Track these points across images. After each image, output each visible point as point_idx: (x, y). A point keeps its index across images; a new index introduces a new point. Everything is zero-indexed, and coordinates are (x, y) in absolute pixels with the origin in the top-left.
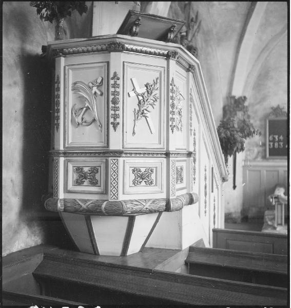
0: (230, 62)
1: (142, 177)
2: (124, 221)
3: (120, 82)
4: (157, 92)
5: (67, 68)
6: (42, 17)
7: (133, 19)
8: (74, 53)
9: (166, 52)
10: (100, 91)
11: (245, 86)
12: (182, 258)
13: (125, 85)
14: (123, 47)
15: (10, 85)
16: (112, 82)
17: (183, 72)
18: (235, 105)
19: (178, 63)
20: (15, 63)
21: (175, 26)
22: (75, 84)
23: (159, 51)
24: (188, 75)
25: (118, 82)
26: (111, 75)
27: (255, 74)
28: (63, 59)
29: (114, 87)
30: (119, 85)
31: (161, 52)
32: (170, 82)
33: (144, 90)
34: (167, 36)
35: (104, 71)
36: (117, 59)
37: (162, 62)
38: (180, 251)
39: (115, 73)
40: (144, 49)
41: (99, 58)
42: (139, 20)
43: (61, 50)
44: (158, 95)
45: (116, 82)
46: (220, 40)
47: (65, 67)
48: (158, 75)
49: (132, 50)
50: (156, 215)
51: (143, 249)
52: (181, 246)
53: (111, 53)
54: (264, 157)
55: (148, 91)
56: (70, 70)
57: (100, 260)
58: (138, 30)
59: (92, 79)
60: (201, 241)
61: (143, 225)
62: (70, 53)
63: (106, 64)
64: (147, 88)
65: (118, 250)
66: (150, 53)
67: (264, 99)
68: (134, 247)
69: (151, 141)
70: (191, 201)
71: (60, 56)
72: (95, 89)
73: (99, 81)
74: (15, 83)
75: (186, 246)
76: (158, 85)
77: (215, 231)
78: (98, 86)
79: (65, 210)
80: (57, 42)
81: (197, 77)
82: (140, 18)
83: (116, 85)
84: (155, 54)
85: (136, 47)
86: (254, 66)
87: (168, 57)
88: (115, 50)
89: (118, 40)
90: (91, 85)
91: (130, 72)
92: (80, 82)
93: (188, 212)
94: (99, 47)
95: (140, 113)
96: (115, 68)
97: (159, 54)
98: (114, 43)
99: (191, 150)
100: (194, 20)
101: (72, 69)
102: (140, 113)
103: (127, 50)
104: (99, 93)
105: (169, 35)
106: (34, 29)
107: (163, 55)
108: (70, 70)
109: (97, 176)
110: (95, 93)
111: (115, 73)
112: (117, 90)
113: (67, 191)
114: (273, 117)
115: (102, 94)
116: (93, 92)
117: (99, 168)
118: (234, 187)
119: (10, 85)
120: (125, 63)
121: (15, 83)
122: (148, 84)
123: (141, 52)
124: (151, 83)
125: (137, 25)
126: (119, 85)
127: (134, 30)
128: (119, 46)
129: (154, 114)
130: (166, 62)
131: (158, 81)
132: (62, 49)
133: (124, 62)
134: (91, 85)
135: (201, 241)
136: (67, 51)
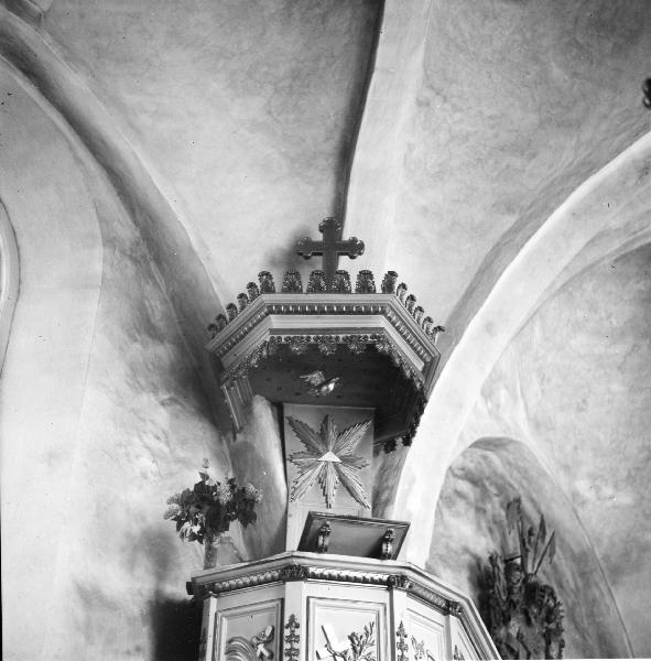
3: (301, 632)
4: (374, 648)
5: (219, 615)
6: (183, 536)
7: (317, 524)
8: (230, 589)
9: (385, 578)
10: (269, 650)
13: (311, 638)
14: (305, 570)
15: (128, 653)
16: (287, 632)
17: (437, 616)
19: (412, 593)
20: (142, 614)
21: (391, 532)
22: (230, 641)
23: (364, 574)
24: (448, 621)
25: (297, 632)
26: (286, 622)
28: (213, 602)
29: (290, 642)
30: (298, 636)
31: (376, 577)
32: (396, 630)
33: (347, 645)
34: (317, 542)
35: (275, 614)
36: (297, 592)
37: (381, 594)
39: (292, 617)
40: (344, 573)
41: (266, 595)
42: (328, 526)
43: (212, 586)
44: (374, 655)
45: (293, 631)
47: (216, 614)
48: (373, 618)
49: (322, 577)
53: (287, 583)
55: (354, 648)
56: (224, 619)
58: (326, 543)
59: (256, 631)
62: (226, 590)
63: (279, 602)
64: (353, 642)
66: (356, 580)
71: (210, 596)
72: (261, 648)
73: (268, 633)
74: (138, 649)
76: (374, 637)
78: (266, 643)
80: (207, 572)
81: (471, 626)
82: (328, 523)
83: (294, 638)
84: (365, 581)
85: (330, 571)
87: (390, 584)
88: (294, 578)
89: (296, 562)
90: (255, 641)
91: (319, 614)
92: (241, 638)
94: (269, 576)
96: (295, 607)
97: (373, 582)
98: (291, 567)
100: (537, 531)
101: (226, 617)
103: (314, 576)
104: (266, 654)
105: (384, 547)
106: (182, 559)
107: (381, 582)
108: (224, 619)
110: (262, 655)
111: (292, 617)
112: (296, 646)
115: (271, 657)
116: (258, 654)
119: (128, 653)
120: (311, 600)
121: (138, 649)
122: (353, 634)
123: (340, 579)
124: (360, 632)
125: (326, 534)
126: (298, 636)
127: (321, 542)
128: (299, 570)
130: (388, 594)
131: (374, 629)
132: (213, 584)
133: (308, 598)
134: (255, 641)
136: (220, 587)
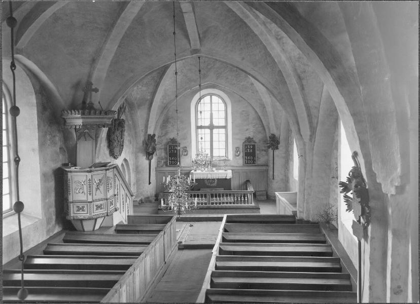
0: (145, 116)
1: (98, 207)
2: (94, 221)
11: (155, 128)
12: (113, 229)
18: (151, 138)
27: (161, 121)
38: (112, 227)
46: (139, 106)
50: (103, 218)
51: (100, 227)
52: (113, 225)
54: (167, 165)
57: (85, 233)
60: (122, 221)
61: (99, 221)
65: (92, 229)
67: (166, 134)
68: (97, 227)
69: (102, 196)
70: (116, 210)
72: (82, 183)
75: (115, 224)
77: (128, 216)
79: (74, 219)
86: (160, 116)
93: (115, 214)
95: (98, 189)
99: (116, 193)
102: (98, 189)
109: (84, 208)
113: (74, 213)
114: (170, 144)
117: (86, 212)
118: (150, 183)
129: (102, 188)
135: (122, 221)
